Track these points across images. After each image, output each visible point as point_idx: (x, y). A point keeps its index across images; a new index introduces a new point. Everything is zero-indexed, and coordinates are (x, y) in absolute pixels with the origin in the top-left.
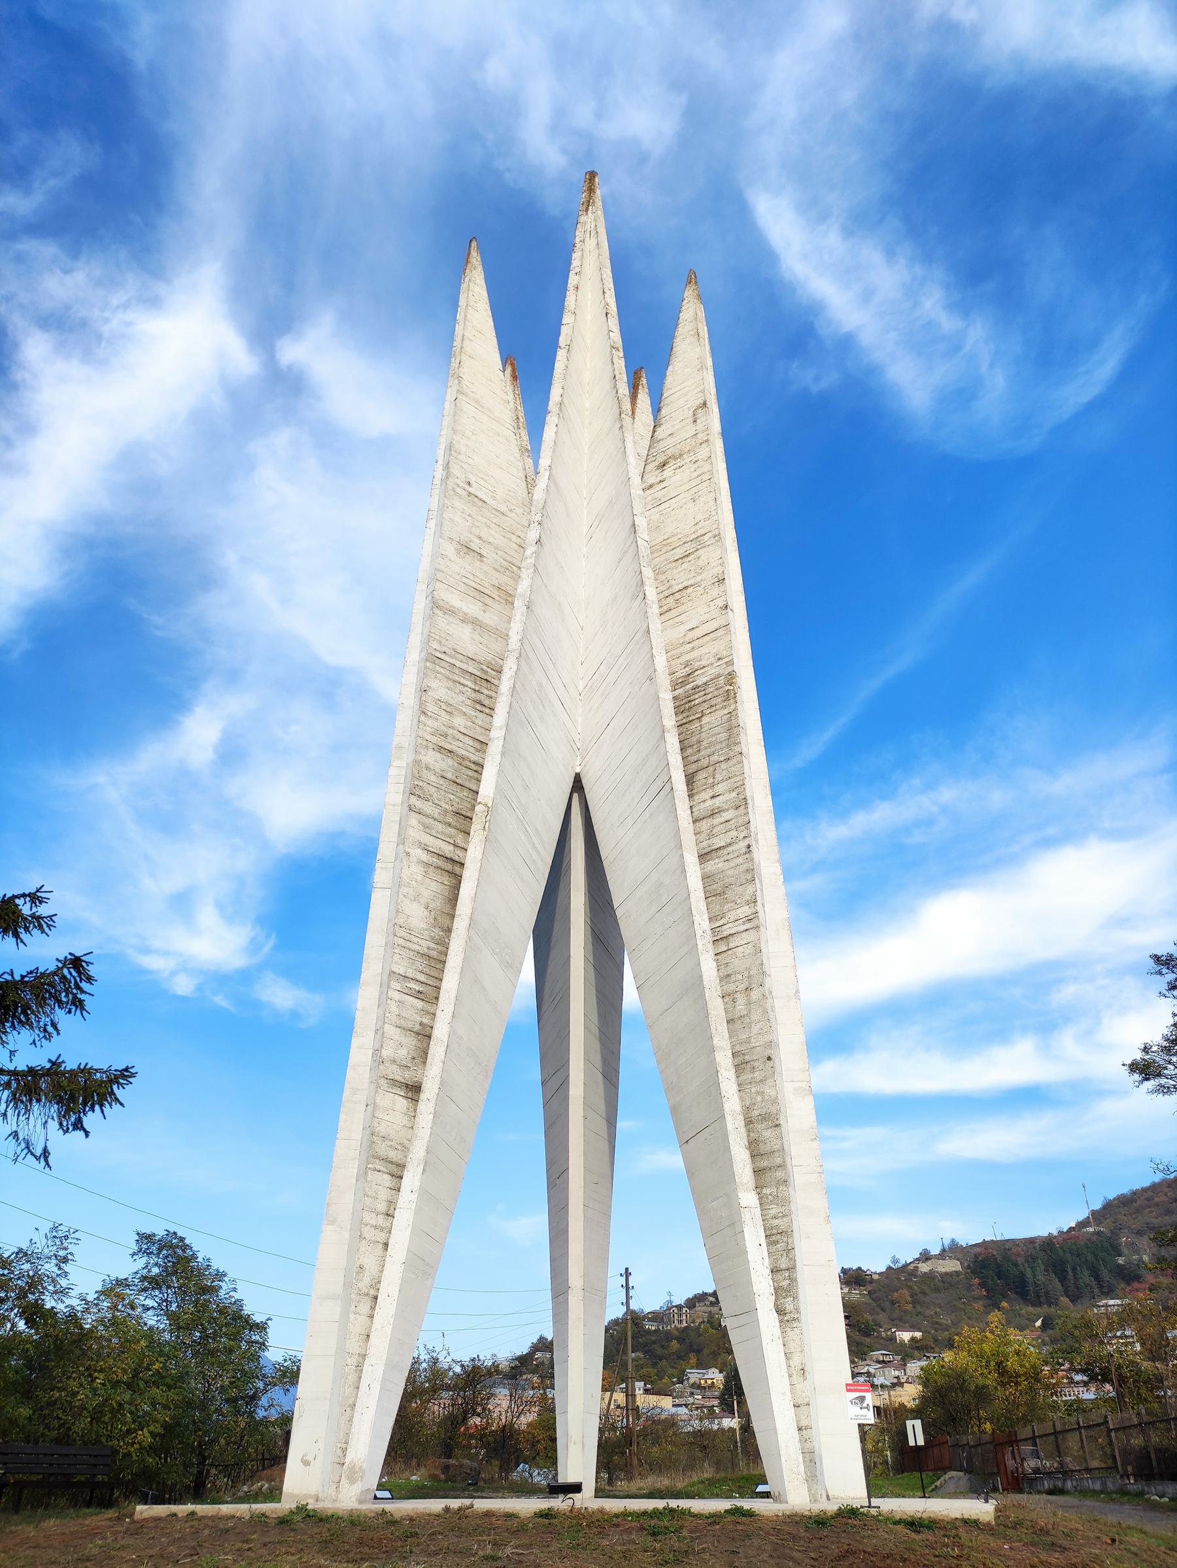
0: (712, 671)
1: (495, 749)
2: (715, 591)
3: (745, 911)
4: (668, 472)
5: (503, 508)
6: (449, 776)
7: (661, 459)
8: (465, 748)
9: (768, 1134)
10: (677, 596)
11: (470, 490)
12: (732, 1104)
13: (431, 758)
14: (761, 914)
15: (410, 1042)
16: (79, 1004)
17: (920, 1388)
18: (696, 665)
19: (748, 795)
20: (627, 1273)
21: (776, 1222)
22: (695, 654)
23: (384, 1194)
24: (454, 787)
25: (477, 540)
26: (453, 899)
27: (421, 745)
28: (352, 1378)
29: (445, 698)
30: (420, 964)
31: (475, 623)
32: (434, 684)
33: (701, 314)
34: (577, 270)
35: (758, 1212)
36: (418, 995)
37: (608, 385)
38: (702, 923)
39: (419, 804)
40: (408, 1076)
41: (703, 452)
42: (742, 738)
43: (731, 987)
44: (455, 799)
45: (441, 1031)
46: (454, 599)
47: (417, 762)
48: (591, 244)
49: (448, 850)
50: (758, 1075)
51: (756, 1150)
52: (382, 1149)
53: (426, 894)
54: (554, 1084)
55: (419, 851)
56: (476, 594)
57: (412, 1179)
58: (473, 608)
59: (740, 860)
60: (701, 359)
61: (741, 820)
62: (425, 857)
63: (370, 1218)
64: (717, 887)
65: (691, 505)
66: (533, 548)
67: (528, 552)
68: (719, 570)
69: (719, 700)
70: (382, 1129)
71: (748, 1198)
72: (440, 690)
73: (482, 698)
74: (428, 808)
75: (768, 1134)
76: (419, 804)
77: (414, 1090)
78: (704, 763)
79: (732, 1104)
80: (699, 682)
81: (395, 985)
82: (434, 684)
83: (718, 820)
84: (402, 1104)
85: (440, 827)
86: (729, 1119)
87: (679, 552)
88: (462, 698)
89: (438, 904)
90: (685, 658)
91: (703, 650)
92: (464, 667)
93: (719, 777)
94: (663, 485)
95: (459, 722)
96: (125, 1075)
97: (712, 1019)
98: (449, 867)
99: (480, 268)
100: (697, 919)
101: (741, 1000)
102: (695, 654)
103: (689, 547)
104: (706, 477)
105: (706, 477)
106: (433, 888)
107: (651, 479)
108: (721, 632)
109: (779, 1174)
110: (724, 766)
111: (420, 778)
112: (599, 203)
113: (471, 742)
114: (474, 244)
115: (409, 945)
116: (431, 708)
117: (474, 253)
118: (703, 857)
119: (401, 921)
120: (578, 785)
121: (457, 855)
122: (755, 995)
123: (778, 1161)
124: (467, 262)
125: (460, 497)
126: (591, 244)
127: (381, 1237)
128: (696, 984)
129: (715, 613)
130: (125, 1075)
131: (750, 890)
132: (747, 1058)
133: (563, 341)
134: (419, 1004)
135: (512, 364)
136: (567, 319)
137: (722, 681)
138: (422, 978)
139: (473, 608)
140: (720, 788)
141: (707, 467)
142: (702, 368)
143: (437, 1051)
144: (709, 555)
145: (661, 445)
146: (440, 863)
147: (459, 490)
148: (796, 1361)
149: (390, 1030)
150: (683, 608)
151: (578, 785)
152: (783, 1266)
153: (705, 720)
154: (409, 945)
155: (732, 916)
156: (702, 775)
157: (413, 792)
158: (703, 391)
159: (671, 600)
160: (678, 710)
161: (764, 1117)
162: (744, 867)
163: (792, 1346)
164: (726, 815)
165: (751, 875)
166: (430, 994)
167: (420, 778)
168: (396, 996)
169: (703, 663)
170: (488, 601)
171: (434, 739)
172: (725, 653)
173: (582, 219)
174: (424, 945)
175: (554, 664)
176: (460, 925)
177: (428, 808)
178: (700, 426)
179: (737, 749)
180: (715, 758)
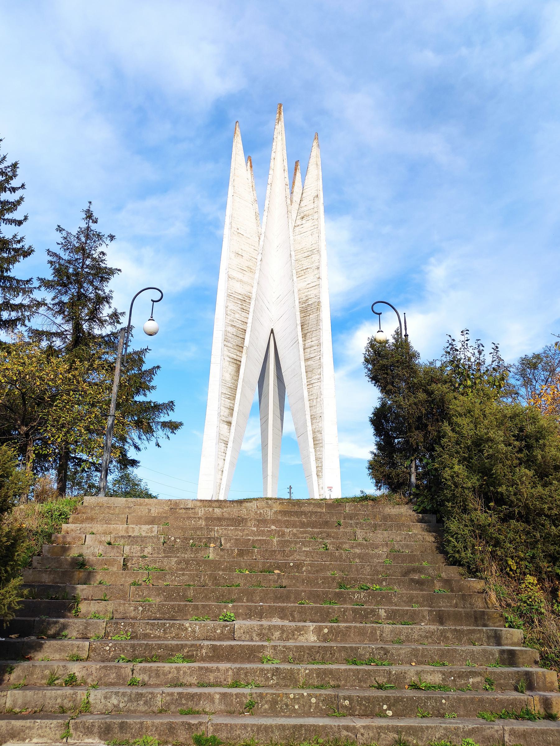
0: (314, 300)
1: (249, 325)
2: (316, 272)
3: (318, 376)
4: (304, 222)
5: (249, 236)
6: (235, 334)
7: (302, 215)
8: (239, 325)
9: (319, 435)
10: (305, 271)
12: (309, 428)
13: (230, 329)
14: (322, 378)
15: (227, 411)
16: (173, 410)
18: (309, 297)
19: (321, 341)
20: (291, 488)
22: (309, 293)
23: (223, 448)
24: (236, 337)
25: (241, 250)
26: (238, 376)
27: (227, 325)
28: (218, 487)
29: (232, 308)
30: (229, 390)
31: (241, 281)
32: (229, 304)
33: (319, 154)
34: (274, 150)
35: (314, 453)
36: (229, 398)
37: (284, 199)
38: (305, 381)
39: (227, 344)
40: (227, 420)
41: (316, 217)
42: (321, 324)
43: (312, 397)
44: (238, 341)
45: (236, 409)
46: (235, 274)
47: (226, 331)
48: (280, 137)
49: (235, 357)
51: (315, 439)
52: (222, 437)
53: (230, 370)
54: (264, 420)
56: (241, 271)
57: (230, 444)
58: (240, 276)
59: (317, 362)
60: (318, 175)
61: (319, 350)
62: (229, 359)
63: (220, 453)
64: (311, 369)
65: (310, 236)
66: (260, 263)
67: (258, 264)
68: (317, 264)
69: (315, 310)
70: (222, 433)
71: (312, 450)
72: (232, 306)
73: (243, 307)
74: (229, 345)
75: (319, 435)
76: (227, 344)
77: (229, 423)
78: (309, 330)
79: (309, 428)
80: (310, 303)
81: (223, 396)
82: (229, 304)
83: (312, 349)
84: (226, 427)
85: (233, 350)
86: (309, 432)
87: (306, 254)
88: (238, 308)
89: (233, 373)
90: (306, 294)
91: (311, 292)
92: (238, 297)
93: (313, 336)
94: (302, 226)
95: (237, 316)
96: (181, 424)
97: (306, 406)
98: (235, 362)
99: (240, 136)
100: (303, 380)
101: (315, 401)
102: (309, 293)
104: (316, 227)
105: (316, 227)
106: (231, 368)
107: (299, 222)
108: (317, 287)
109: (321, 445)
110: (315, 332)
111: (226, 336)
112: (282, 119)
113: (240, 322)
114: (237, 124)
116: (229, 312)
117: (237, 129)
118: (306, 360)
119: (223, 378)
120: (272, 331)
121: (238, 358)
122: (318, 400)
124: (235, 133)
125: (235, 235)
126: (279, 143)
127: (223, 458)
128: (302, 398)
129: (316, 280)
130: (181, 424)
131: (319, 370)
134: (229, 401)
135: (250, 160)
137: (316, 304)
138: (230, 394)
139: (240, 276)
140: (313, 339)
141: (316, 223)
142: (318, 179)
144: (315, 257)
145: (302, 209)
146: (233, 361)
148: (321, 486)
149: (222, 408)
150: (306, 276)
151: (272, 331)
153: (311, 316)
155: (314, 378)
156: (308, 334)
157: (225, 340)
158: (317, 190)
161: (318, 431)
163: (320, 483)
164: (315, 348)
165: (320, 366)
166: (233, 398)
167: (226, 336)
168: (223, 399)
169: (311, 297)
170: (245, 272)
172: (318, 294)
173: (277, 127)
174: (230, 385)
176: (240, 380)
177: (229, 345)
179: (319, 327)
180: (313, 329)
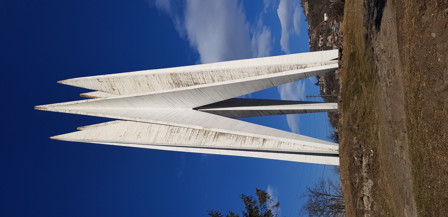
2: (149, 77)
3: (226, 72)
9: (272, 69)
24: (198, 136)
62: (215, 141)
83: (205, 78)
87: (138, 86)
102: (165, 82)
103: (137, 83)
118: (214, 81)
133: (86, 114)
138: (241, 140)
140: (198, 77)
143: (257, 136)
145: (108, 90)
146: (216, 138)
159: (151, 88)
160: (179, 86)
164: (204, 76)
180: (191, 78)
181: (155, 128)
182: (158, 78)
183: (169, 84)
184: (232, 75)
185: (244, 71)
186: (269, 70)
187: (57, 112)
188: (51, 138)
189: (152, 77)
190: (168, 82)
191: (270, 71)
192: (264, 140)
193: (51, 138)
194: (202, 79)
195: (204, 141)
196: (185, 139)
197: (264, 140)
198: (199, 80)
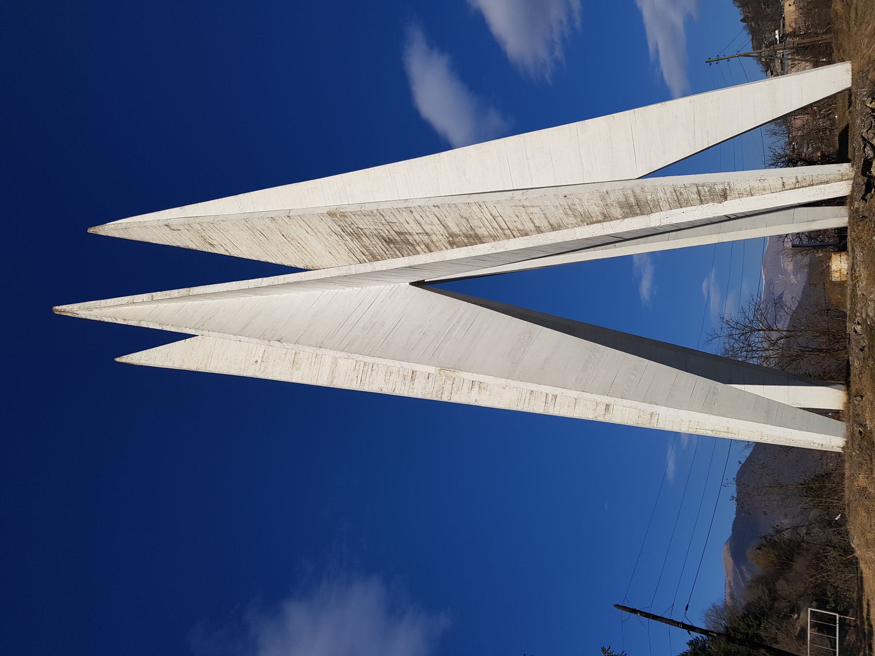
9: (613, 197)
11: (259, 361)
17: (833, 280)
21: (668, 193)
50: (577, 202)
55: (473, 393)
83: (421, 220)
103: (258, 234)
115: (527, 400)
123: (630, 192)
132: (567, 207)
136: (144, 325)
140: (402, 220)
147: (262, 369)
152: (696, 190)
153: (361, 226)
154: (527, 400)
159: (293, 242)
162: (448, 209)
169: (327, 227)
171: (408, 383)
175: (349, 316)
178: (181, 228)
180: (384, 222)
181: (328, 355)
182: (301, 222)
183: (333, 234)
184: (495, 213)
185: (526, 204)
186: (603, 199)
187: (100, 321)
188: (118, 360)
189: (287, 220)
190: (329, 230)
191: (609, 201)
192: (608, 406)
193: (118, 360)
194: (413, 224)
195: (448, 387)
196: (401, 378)
197: (608, 406)
198: (408, 227)
